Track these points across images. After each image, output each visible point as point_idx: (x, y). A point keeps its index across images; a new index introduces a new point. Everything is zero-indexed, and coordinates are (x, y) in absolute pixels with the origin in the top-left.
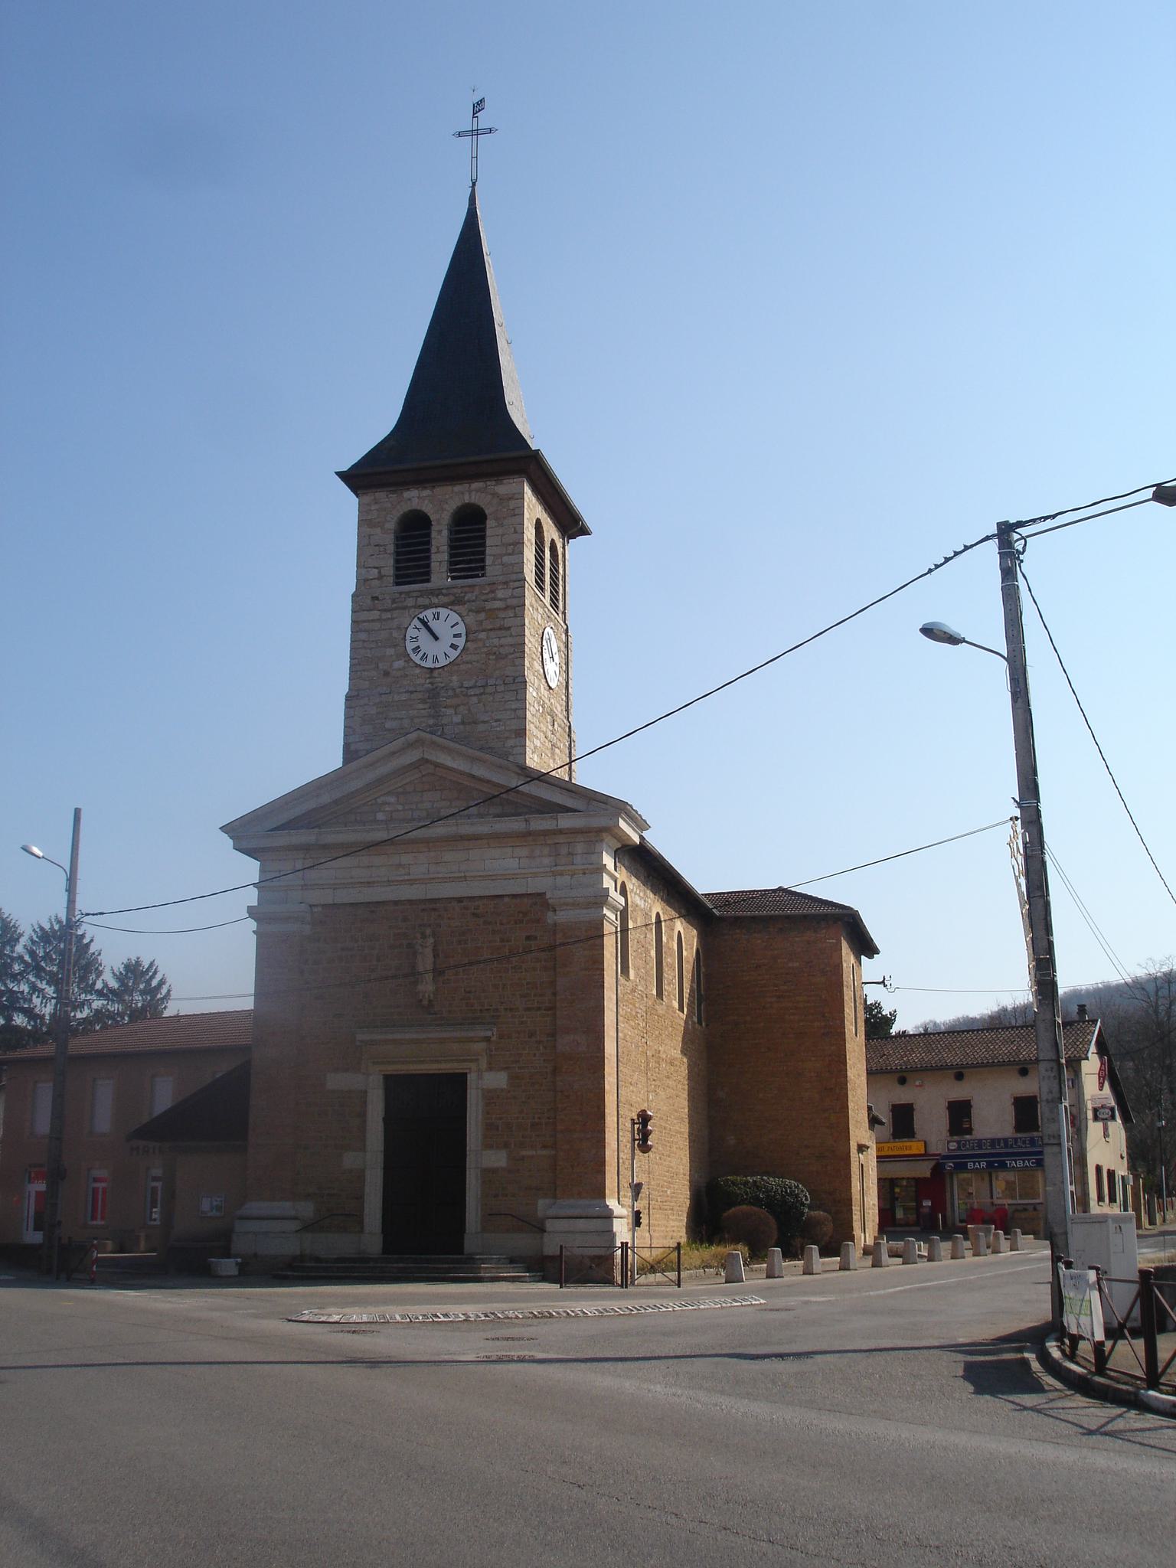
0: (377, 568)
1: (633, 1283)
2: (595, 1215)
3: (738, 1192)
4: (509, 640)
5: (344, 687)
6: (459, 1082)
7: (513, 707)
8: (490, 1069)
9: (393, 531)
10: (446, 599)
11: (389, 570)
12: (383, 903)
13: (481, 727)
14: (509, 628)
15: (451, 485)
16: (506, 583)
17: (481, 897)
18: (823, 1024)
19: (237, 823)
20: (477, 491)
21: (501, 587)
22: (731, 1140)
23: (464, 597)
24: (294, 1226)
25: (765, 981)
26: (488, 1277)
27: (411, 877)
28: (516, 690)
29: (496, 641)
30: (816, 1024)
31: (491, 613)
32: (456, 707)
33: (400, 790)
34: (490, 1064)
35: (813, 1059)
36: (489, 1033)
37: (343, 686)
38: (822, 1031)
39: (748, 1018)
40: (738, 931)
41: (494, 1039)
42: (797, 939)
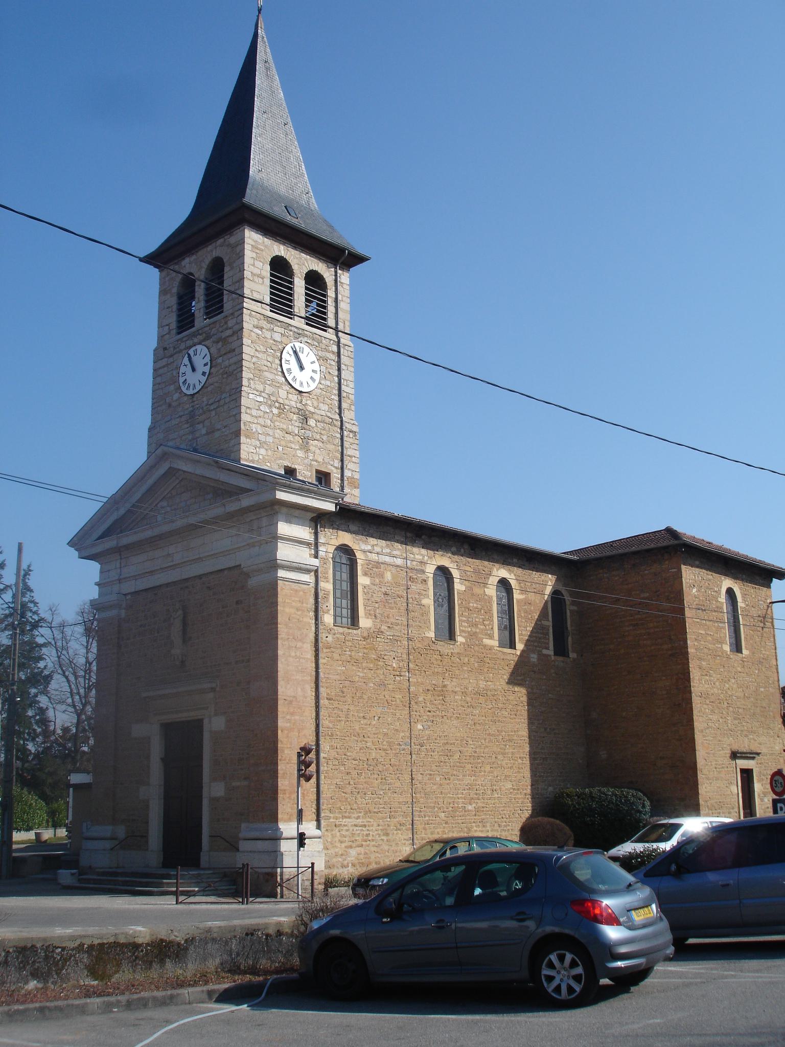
0: (167, 325)
1: (282, 897)
2: (268, 837)
3: (570, 803)
4: (232, 361)
5: (148, 422)
6: (198, 725)
7: (234, 413)
8: (216, 715)
9: (176, 294)
10: (200, 337)
11: (174, 325)
12: (160, 586)
13: (217, 434)
14: (234, 350)
15: (205, 247)
16: (232, 314)
17: (211, 573)
18: (670, 646)
19: (75, 539)
20: (221, 246)
21: (231, 318)
22: (603, 755)
23: (210, 333)
24: (108, 845)
25: (623, 613)
26: (157, 892)
27: (174, 563)
28: (236, 399)
29: (227, 363)
30: (665, 647)
31: (224, 341)
32: (203, 422)
33: (169, 495)
34: (216, 710)
35: (664, 678)
36: (214, 685)
37: (147, 421)
38: (670, 652)
39: (612, 646)
40: (601, 571)
41: (218, 689)
42: (646, 572)
